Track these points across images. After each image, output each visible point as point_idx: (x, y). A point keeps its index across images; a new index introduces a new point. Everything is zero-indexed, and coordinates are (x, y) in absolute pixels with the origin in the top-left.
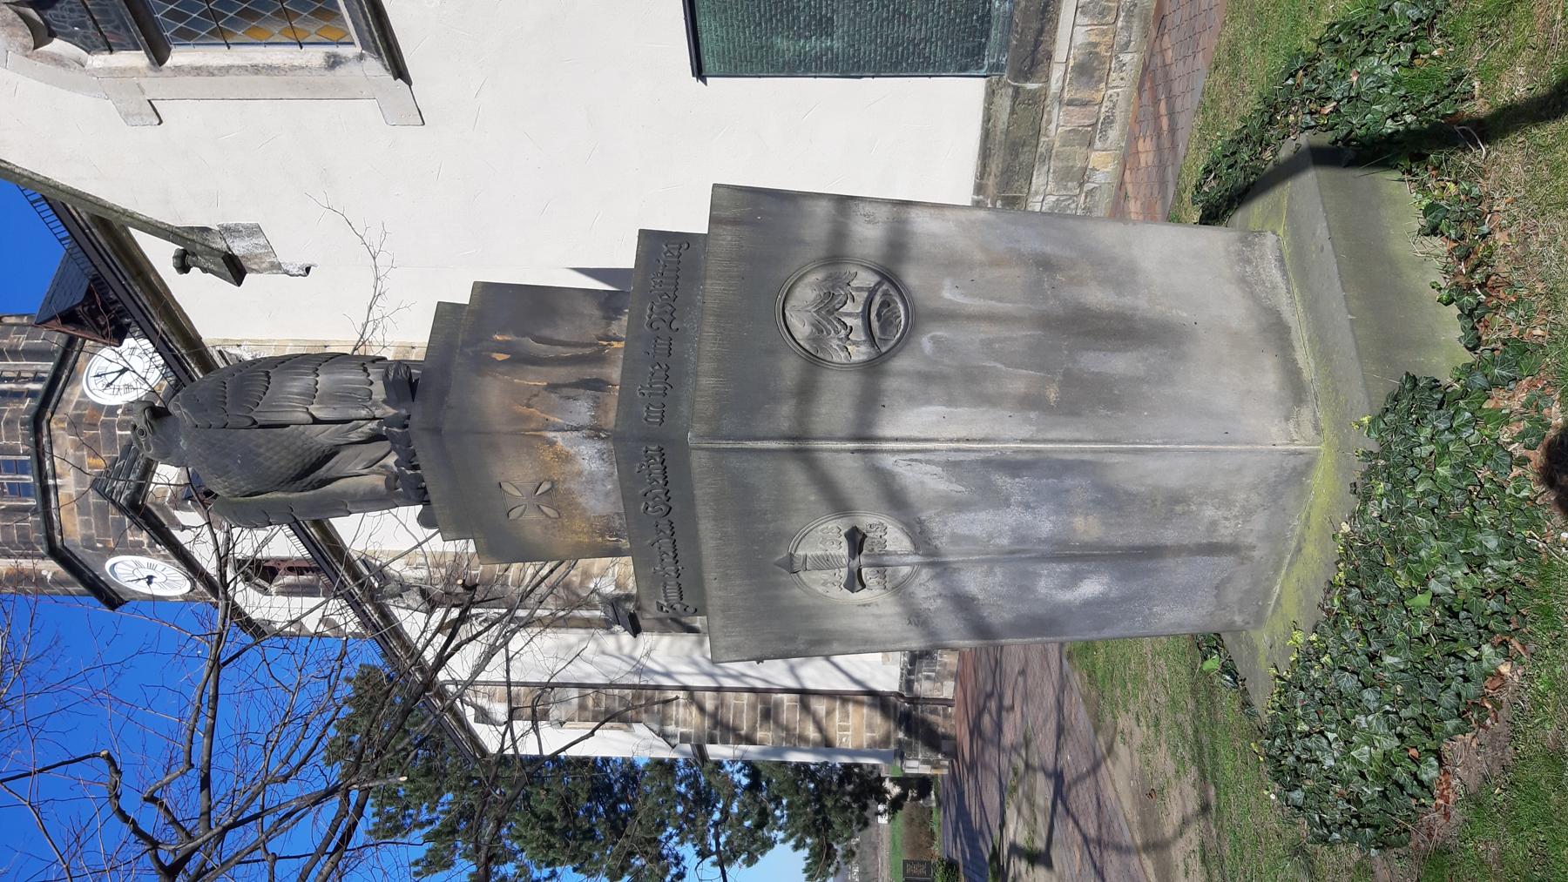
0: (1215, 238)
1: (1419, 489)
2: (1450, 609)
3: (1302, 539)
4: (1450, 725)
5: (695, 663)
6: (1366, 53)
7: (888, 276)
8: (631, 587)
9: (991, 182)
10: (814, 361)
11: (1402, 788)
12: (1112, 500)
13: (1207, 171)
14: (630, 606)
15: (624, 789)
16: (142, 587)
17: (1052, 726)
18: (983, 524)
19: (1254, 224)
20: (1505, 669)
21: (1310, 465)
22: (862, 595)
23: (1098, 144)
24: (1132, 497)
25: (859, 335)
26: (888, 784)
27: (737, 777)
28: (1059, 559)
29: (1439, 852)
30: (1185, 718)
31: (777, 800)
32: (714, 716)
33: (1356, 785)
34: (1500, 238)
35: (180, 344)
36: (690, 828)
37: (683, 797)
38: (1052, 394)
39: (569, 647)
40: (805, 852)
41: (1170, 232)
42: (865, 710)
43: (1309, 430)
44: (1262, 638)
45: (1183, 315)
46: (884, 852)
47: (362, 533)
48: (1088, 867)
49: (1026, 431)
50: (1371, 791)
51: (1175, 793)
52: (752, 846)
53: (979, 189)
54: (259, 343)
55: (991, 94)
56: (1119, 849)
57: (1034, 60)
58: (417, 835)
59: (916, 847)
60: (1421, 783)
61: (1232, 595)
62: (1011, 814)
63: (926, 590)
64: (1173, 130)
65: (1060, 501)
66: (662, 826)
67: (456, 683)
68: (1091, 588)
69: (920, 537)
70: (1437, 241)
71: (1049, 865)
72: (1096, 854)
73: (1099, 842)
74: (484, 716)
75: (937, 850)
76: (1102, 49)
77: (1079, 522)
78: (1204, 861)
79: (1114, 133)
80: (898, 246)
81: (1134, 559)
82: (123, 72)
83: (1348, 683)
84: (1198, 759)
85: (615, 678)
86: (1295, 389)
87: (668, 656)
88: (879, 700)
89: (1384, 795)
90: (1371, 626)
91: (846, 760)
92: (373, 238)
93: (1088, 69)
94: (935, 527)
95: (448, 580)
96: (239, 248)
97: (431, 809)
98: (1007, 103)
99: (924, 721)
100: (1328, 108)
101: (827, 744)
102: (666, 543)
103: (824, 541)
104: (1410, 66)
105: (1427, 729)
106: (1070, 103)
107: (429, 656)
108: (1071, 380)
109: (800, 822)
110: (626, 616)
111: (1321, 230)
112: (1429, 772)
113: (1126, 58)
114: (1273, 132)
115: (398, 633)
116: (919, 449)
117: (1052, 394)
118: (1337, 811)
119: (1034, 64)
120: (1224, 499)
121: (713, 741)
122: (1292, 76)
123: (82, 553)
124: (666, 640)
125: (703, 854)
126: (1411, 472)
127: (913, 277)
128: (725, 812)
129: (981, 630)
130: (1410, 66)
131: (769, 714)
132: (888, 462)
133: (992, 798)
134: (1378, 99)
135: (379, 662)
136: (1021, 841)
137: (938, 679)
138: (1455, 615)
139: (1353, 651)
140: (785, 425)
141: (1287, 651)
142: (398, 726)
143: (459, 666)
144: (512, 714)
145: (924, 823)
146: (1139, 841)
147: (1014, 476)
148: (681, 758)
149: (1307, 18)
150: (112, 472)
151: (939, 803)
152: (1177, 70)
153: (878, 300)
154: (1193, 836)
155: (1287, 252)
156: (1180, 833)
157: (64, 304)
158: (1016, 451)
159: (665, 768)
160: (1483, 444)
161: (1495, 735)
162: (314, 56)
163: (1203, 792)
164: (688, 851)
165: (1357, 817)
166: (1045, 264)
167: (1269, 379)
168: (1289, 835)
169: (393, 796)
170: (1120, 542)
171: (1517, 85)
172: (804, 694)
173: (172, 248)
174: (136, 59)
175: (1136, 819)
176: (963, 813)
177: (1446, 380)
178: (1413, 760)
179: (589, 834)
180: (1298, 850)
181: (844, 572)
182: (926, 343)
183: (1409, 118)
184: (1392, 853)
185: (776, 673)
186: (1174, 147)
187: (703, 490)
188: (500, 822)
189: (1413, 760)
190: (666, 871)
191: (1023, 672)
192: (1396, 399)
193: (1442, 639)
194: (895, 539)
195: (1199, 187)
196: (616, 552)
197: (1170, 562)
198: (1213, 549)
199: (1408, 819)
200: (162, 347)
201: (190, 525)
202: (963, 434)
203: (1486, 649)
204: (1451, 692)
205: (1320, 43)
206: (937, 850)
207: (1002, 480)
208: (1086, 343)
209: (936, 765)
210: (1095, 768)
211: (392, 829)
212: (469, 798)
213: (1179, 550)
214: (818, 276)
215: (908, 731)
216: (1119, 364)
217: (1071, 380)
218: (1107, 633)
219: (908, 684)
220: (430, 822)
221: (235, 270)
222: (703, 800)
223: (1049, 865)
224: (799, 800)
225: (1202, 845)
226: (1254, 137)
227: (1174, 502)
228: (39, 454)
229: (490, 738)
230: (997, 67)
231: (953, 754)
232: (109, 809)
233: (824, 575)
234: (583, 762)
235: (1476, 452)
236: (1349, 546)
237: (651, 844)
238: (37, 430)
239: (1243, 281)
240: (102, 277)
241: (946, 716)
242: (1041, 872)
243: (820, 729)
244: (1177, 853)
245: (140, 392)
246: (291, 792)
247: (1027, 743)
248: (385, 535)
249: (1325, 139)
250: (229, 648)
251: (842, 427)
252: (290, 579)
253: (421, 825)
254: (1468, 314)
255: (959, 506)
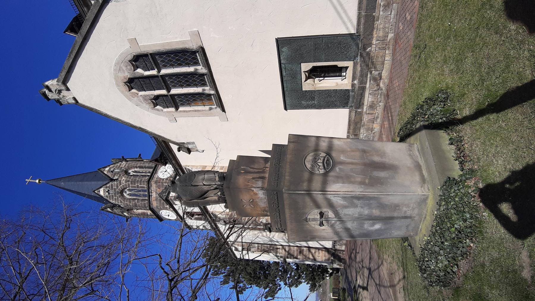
0: (403, 145)
1: (452, 203)
2: (459, 231)
3: (426, 215)
4: (460, 258)
5: (284, 239)
6: (434, 105)
7: (328, 154)
8: (269, 221)
9: (351, 131)
10: (312, 173)
11: (449, 273)
12: (382, 206)
13: (400, 130)
14: (269, 226)
15: (267, 268)
16: (167, 217)
17: (368, 257)
18: (350, 211)
19: (412, 142)
20: (472, 245)
21: (427, 198)
22: (323, 227)
23: (375, 123)
24: (387, 205)
25: (322, 167)
26: (329, 270)
27: (294, 267)
28: (370, 220)
29: (457, 287)
30: (400, 256)
31: (303, 272)
32: (288, 252)
33: (439, 272)
34: (466, 146)
35: (177, 166)
36: (283, 278)
37: (281, 270)
38: (367, 181)
39: (255, 234)
40: (309, 285)
41: (393, 143)
42: (324, 252)
43: (426, 189)
44: (417, 238)
45: (396, 163)
46: (328, 285)
47: (211, 208)
48: (377, 291)
49: (361, 190)
50: (442, 274)
51: (397, 274)
52: (296, 283)
53: (348, 132)
54: (197, 167)
55: (350, 112)
56: (384, 286)
57: (360, 104)
58: (221, 276)
59: (336, 285)
60: (453, 272)
61: (410, 228)
62: (358, 278)
63: (339, 227)
64: (392, 120)
65: (370, 206)
66: (276, 277)
67: (231, 241)
68: (377, 226)
69: (337, 214)
70: (453, 146)
71: (367, 290)
72: (379, 288)
73: (379, 285)
74: (237, 249)
75: (341, 285)
76: (375, 102)
77: (374, 211)
78: (404, 290)
79: (379, 120)
80: (330, 147)
81: (387, 220)
82: (170, 112)
83: (437, 249)
84: (403, 266)
85: (266, 242)
86: (423, 180)
87: (278, 238)
88: (327, 250)
89: (445, 275)
90: (442, 235)
91: (319, 264)
92: (217, 145)
93: (372, 106)
94: (340, 212)
95: (230, 219)
96: (190, 147)
97: (225, 270)
98: (354, 114)
99: (338, 255)
100: (426, 117)
101: (315, 260)
102: (278, 214)
103: (314, 214)
104: (444, 107)
105: (455, 259)
106: (368, 114)
107: (225, 236)
108: (371, 178)
109: (308, 278)
110: (268, 228)
111: (427, 143)
112: (455, 269)
113: (381, 104)
114: (414, 122)
115: (219, 230)
116: (336, 195)
117: (367, 181)
118: (434, 278)
119: (360, 106)
120: (408, 206)
121: (288, 258)
122: (418, 109)
123: (156, 210)
124: (277, 234)
125: (286, 284)
126: (450, 200)
127: (334, 154)
128: (290, 274)
129: (352, 236)
130: (444, 107)
131: (301, 252)
132: (329, 196)
133: (354, 274)
134: (437, 115)
135: (215, 236)
136: (361, 284)
137: (341, 245)
138: (460, 233)
139: (438, 241)
140: (305, 188)
141: (423, 241)
142: (218, 252)
143: (232, 238)
144: (243, 249)
145: (338, 279)
146: (389, 285)
147: (359, 200)
148: (280, 262)
149: (420, 96)
150: (163, 192)
151: (341, 275)
152: (392, 107)
153: (326, 159)
154: (401, 284)
155: (420, 148)
156: (398, 283)
157: (155, 158)
158: (359, 194)
159: (276, 263)
160: (465, 193)
161: (470, 260)
162: (207, 108)
163: (404, 273)
164: (282, 283)
165: (439, 280)
166: (364, 151)
167: (417, 178)
168: (423, 284)
169: (216, 266)
170: (384, 216)
171: (467, 112)
172: (309, 248)
173: (177, 147)
174: (173, 109)
175: (388, 280)
176: (347, 277)
177: (457, 178)
178: (452, 266)
179: (259, 278)
180: (425, 287)
181: (319, 222)
182: (337, 169)
183: (444, 119)
184: (446, 288)
185: (304, 244)
186: (393, 123)
187: (286, 202)
188: (240, 274)
189: (452, 266)
190: (277, 288)
191: (361, 244)
192: (446, 183)
193: (458, 238)
194: (331, 214)
195: (399, 133)
196: (267, 216)
197: (395, 221)
198: (406, 217)
199: (450, 280)
200: (174, 166)
201: (178, 205)
202: (346, 190)
203: (467, 240)
204: (460, 251)
205: (423, 102)
206: (341, 285)
207: (356, 201)
208: (374, 170)
209: (340, 266)
210: (378, 268)
211: (216, 274)
212: (233, 268)
213: (398, 218)
214: (313, 154)
215: (334, 258)
216: (382, 174)
217: (371, 178)
218: (381, 237)
219: (334, 246)
220: (224, 273)
221: (189, 151)
222: (285, 271)
223: (367, 290)
224: (308, 273)
225: (403, 286)
226: (410, 122)
227: (396, 207)
228: (149, 188)
229: (238, 255)
230: (352, 106)
231: (345, 263)
232: (159, 266)
233: (314, 223)
234: (258, 261)
235: (464, 195)
236: (436, 217)
237: (274, 282)
238: (149, 183)
239: (410, 155)
240: (163, 152)
241: (343, 254)
242: (365, 291)
243: (313, 256)
244: (397, 288)
245: (169, 175)
246: (196, 265)
247: (362, 261)
248: (218, 209)
249: (427, 123)
250: (184, 233)
251: (318, 189)
252: (196, 216)
253: (223, 273)
254: (461, 163)
255: (345, 207)
